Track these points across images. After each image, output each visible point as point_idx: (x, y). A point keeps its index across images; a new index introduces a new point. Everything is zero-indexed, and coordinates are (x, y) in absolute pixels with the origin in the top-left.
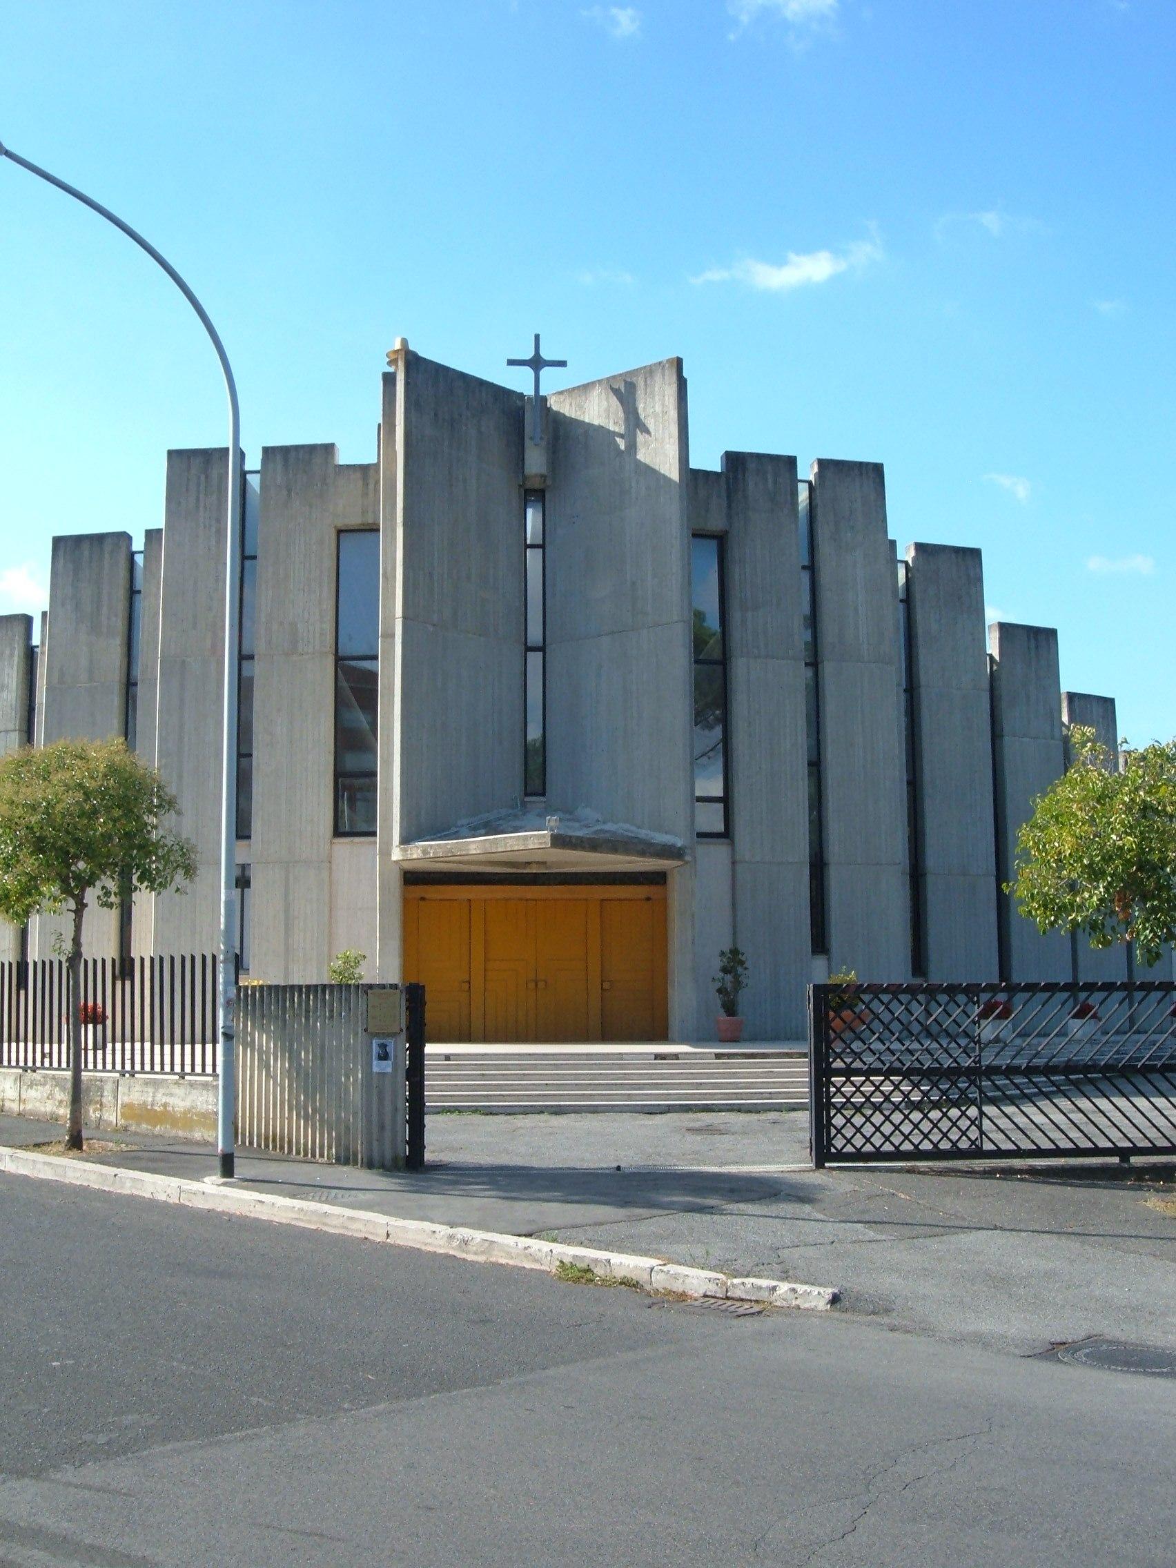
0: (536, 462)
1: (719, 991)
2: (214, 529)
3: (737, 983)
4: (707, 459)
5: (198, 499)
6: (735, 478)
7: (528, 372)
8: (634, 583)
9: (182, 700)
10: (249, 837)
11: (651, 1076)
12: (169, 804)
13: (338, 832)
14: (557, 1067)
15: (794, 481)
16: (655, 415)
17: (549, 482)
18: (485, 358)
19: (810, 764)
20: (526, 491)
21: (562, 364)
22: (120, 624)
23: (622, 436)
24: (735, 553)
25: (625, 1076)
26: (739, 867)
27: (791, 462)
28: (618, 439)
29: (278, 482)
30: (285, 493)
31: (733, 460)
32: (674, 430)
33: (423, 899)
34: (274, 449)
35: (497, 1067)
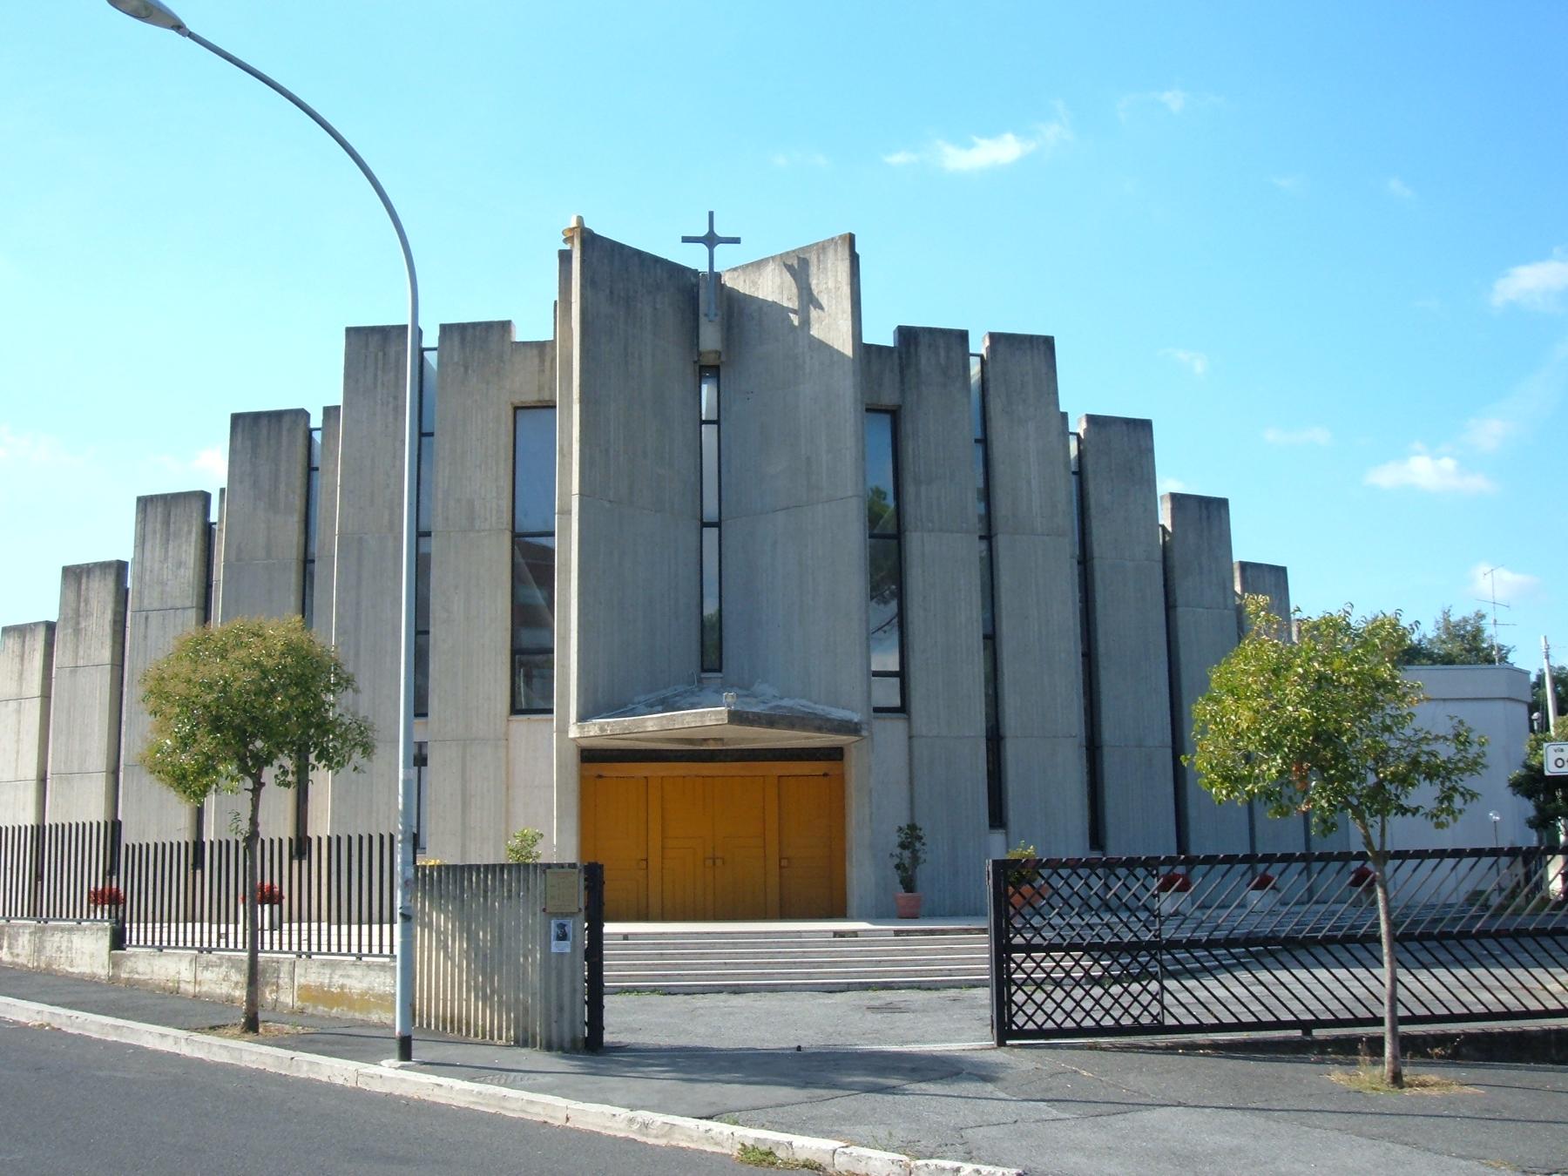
0: (710, 338)
1: (898, 867)
3: (915, 859)
4: (880, 334)
6: (908, 352)
8: (808, 458)
11: (830, 954)
13: (515, 710)
15: (966, 355)
16: (828, 290)
17: (723, 358)
18: (661, 236)
19: (986, 637)
20: (701, 367)
23: (795, 312)
27: (963, 336)
32: (846, 290)
35: (676, 946)
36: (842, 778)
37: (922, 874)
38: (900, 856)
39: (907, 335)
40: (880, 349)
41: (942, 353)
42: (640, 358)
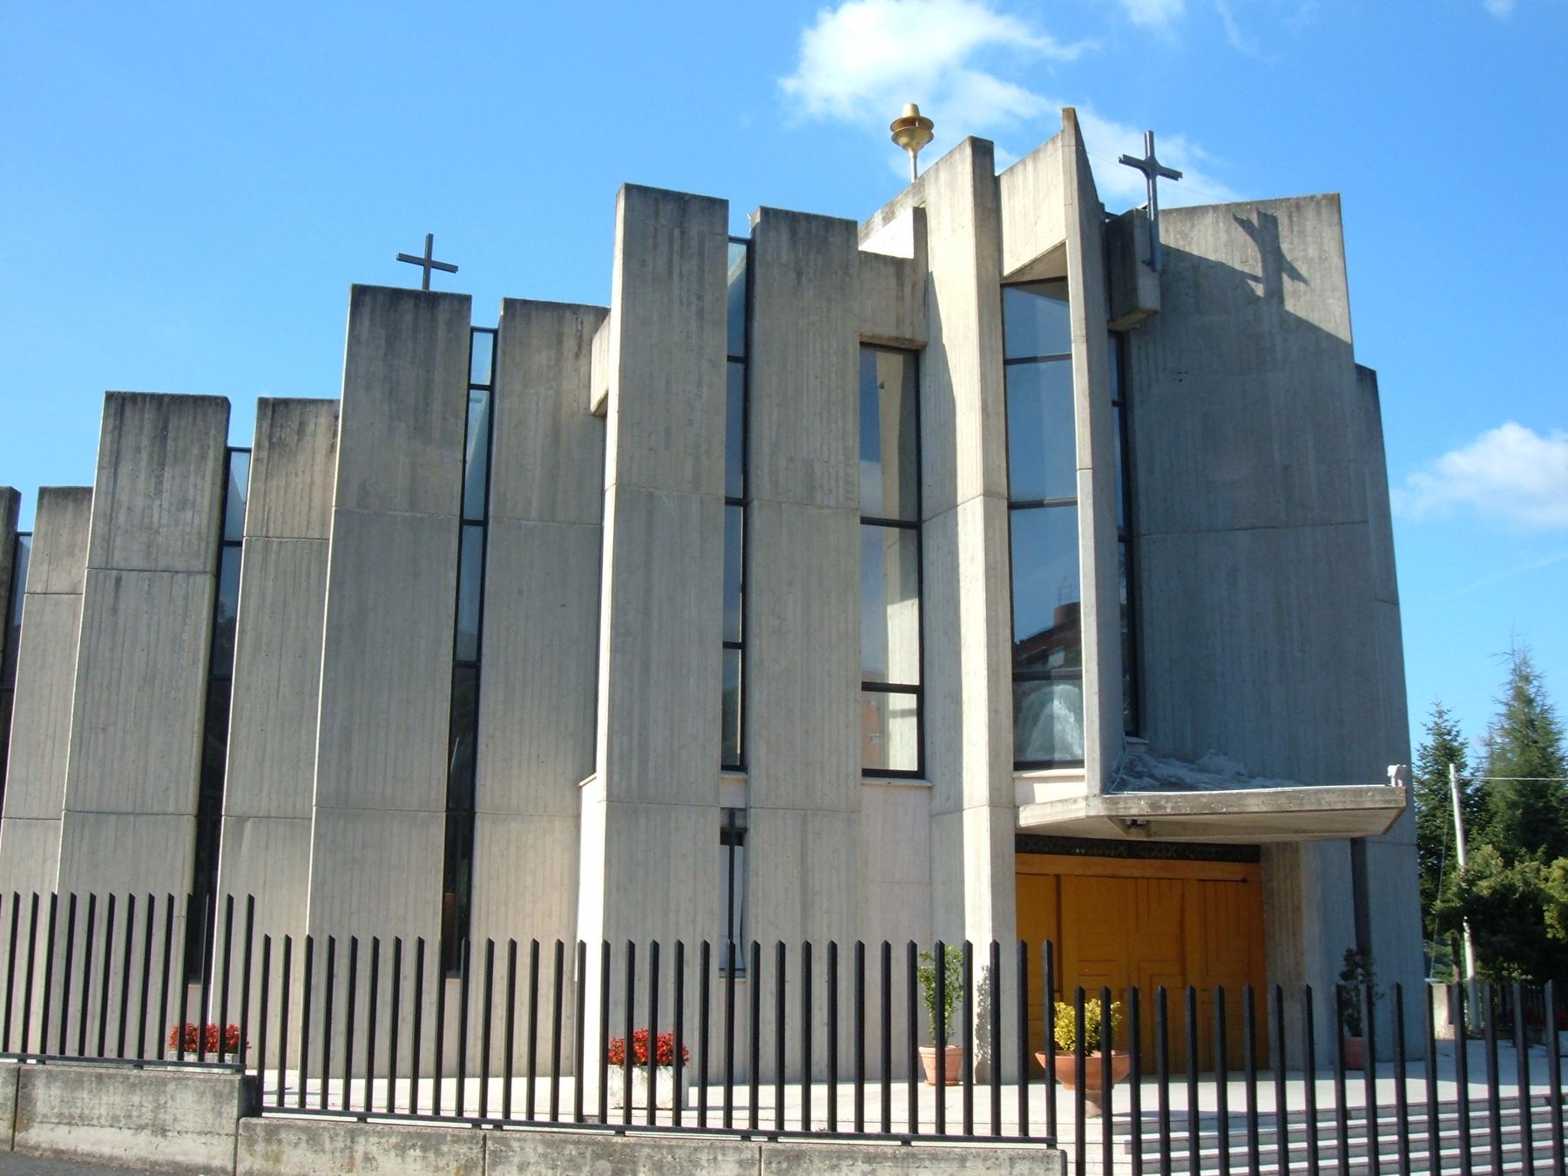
2: (693, 308)
5: (670, 261)
7: (1138, 175)
12: (1502, 728)
16: (1309, 261)
23: (1256, 279)
27: (223, 405)
28: (1252, 284)
30: (793, 275)
34: (777, 212)
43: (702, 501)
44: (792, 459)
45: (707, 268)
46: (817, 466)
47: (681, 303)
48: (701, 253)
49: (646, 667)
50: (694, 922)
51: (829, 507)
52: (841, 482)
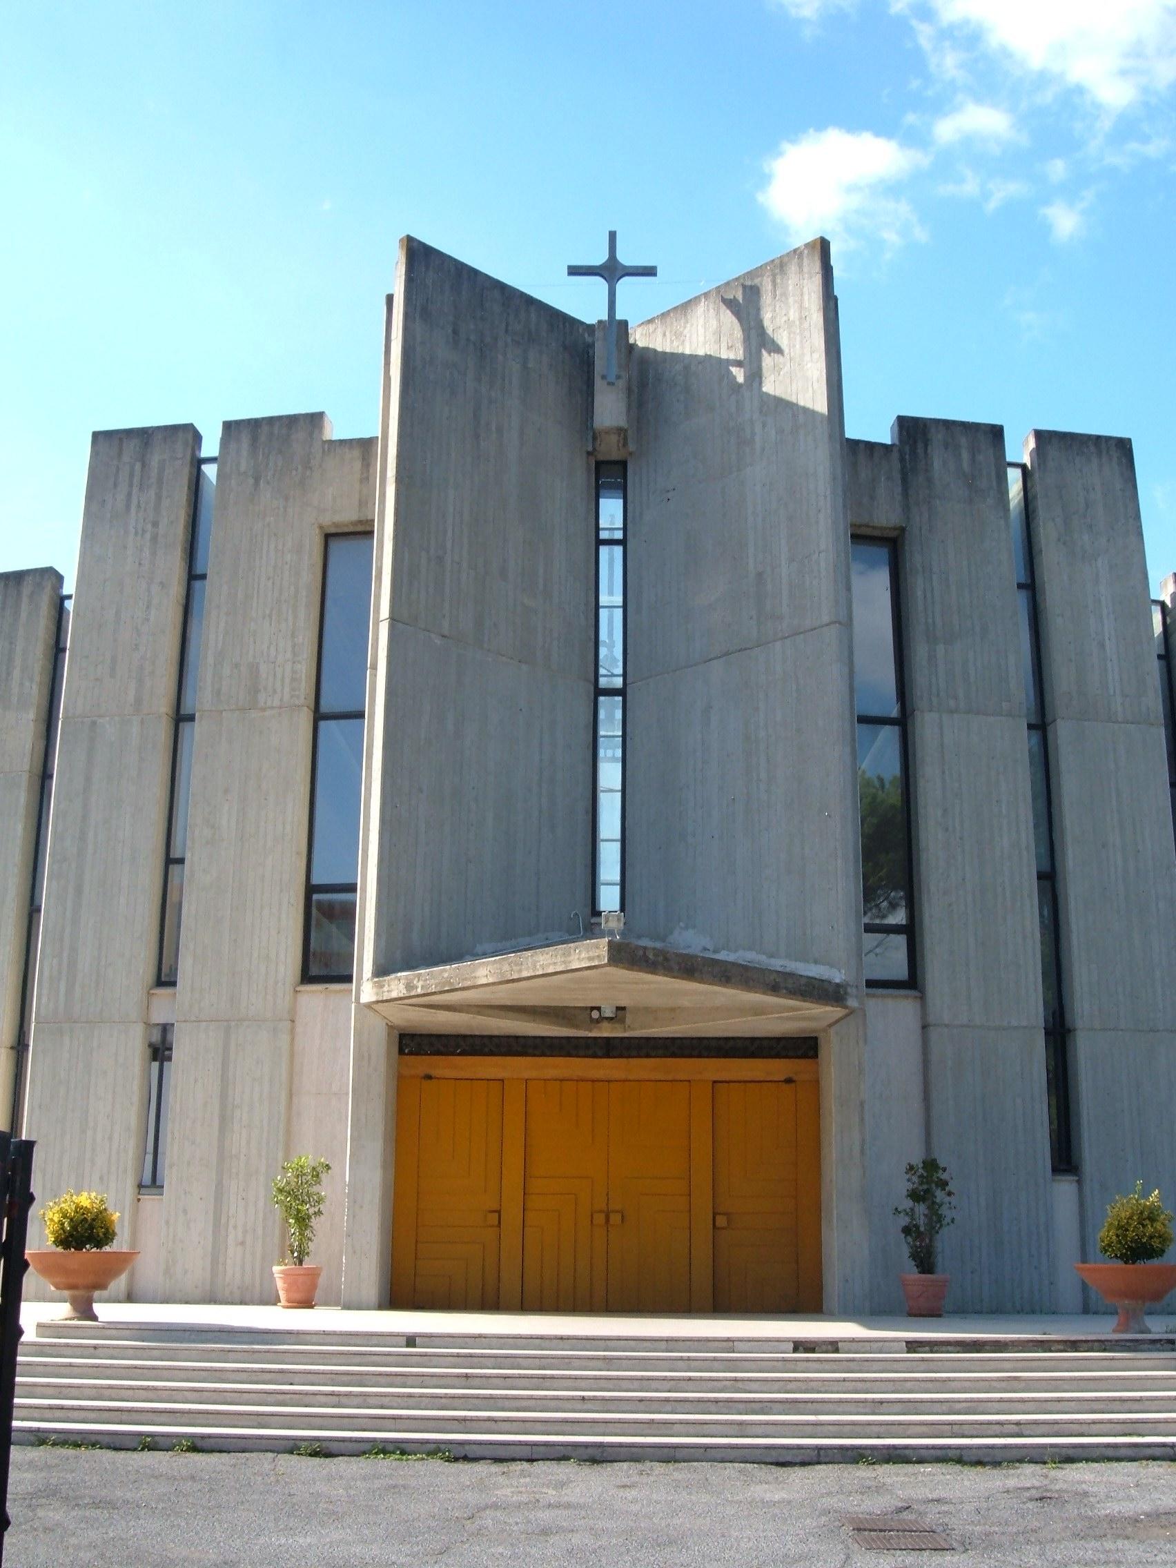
0: (610, 409)
1: (906, 1231)
2: (148, 536)
3: (935, 1218)
4: (871, 423)
5: (129, 495)
6: (913, 452)
7: (599, 285)
8: (760, 575)
9: (88, 779)
10: (173, 984)
11: (784, 1385)
13: (307, 977)
14: (609, 1363)
15: (1002, 465)
17: (632, 447)
18: (535, 263)
19: (1041, 876)
20: (599, 464)
21: (650, 272)
22: (35, 692)
23: (739, 364)
24: (915, 558)
25: (736, 1385)
26: (934, 1034)
27: (996, 432)
28: (734, 370)
29: (243, 468)
30: (251, 481)
31: (911, 429)
32: (818, 340)
33: (429, 1077)
34: (238, 423)
35: (499, 1362)
36: (815, 1085)
37: (946, 1243)
38: (911, 1213)
39: (913, 430)
40: (871, 447)
41: (965, 455)
42: (500, 430)
43: (142, 722)
44: (237, 666)
45: (165, 493)
46: (263, 668)
47: (136, 533)
48: (160, 481)
49: (79, 891)
50: (110, 1139)
51: (272, 708)
52: (287, 681)
